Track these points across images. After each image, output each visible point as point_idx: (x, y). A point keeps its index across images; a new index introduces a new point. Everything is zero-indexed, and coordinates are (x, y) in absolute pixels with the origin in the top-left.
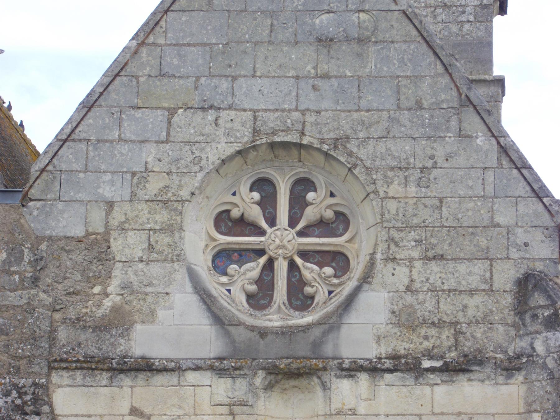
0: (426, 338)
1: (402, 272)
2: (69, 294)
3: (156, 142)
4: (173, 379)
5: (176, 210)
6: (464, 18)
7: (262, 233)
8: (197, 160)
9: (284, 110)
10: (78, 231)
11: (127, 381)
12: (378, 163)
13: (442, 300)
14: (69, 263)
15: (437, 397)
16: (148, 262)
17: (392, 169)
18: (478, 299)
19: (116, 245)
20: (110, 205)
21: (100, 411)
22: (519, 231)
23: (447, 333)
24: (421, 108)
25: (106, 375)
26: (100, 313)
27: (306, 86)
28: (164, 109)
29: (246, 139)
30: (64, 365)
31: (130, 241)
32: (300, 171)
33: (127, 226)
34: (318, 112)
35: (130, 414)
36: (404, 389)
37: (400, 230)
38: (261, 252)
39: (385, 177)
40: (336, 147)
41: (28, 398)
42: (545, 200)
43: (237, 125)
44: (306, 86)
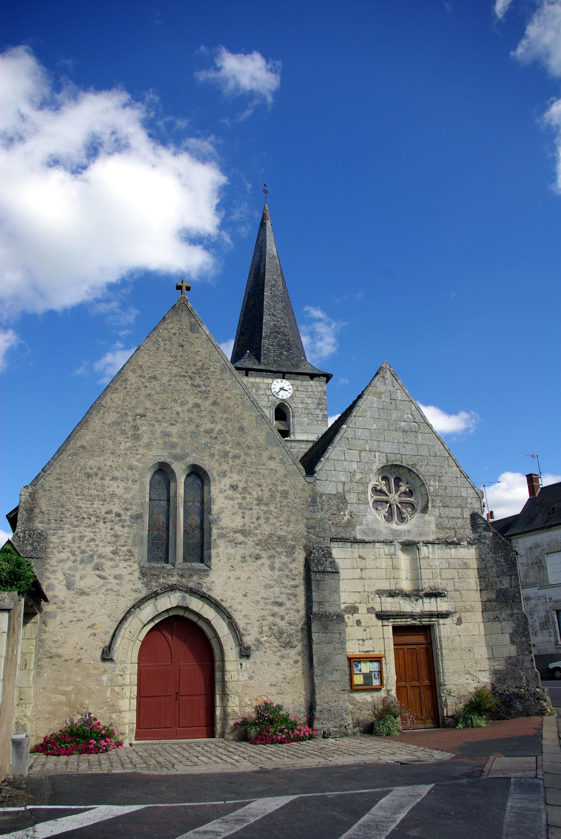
0: (447, 533)
1: (437, 510)
2: (333, 514)
3: (356, 462)
4: (371, 545)
5: (365, 486)
6: (319, 419)
7: (387, 495)
8: (370, 469)
9: (395, 454)
10: (334, 492)
11: (356, 546)
12: (426, 474)
13: (450, 520)
14: (332, 503)
15: (452, 553)
16: (359, 504)
17: (430, 476)
18: (459, 521)
19: (347, 497)
20: (344, 483)
21: (348, 557)
22: (469, 499)
23: (452, 531)
24: (436, 456)
25: (350, 544)
26: (344, 521)
27: (401, 446)
28: (358, 450)
29: (384, 463)
30: (335, 540)
31: (352, 496)
32: (397, 475)
33: (350, 491)
34: (406, 455)
35: (359, 558)
36: (442, 550)
37: (435, 496)
38: (387, 502)
39: (428, 478)
40: (413, 467)
41: (325, 552)
42: (475, 489)
43: (381, 458)
44: (401, 446)
